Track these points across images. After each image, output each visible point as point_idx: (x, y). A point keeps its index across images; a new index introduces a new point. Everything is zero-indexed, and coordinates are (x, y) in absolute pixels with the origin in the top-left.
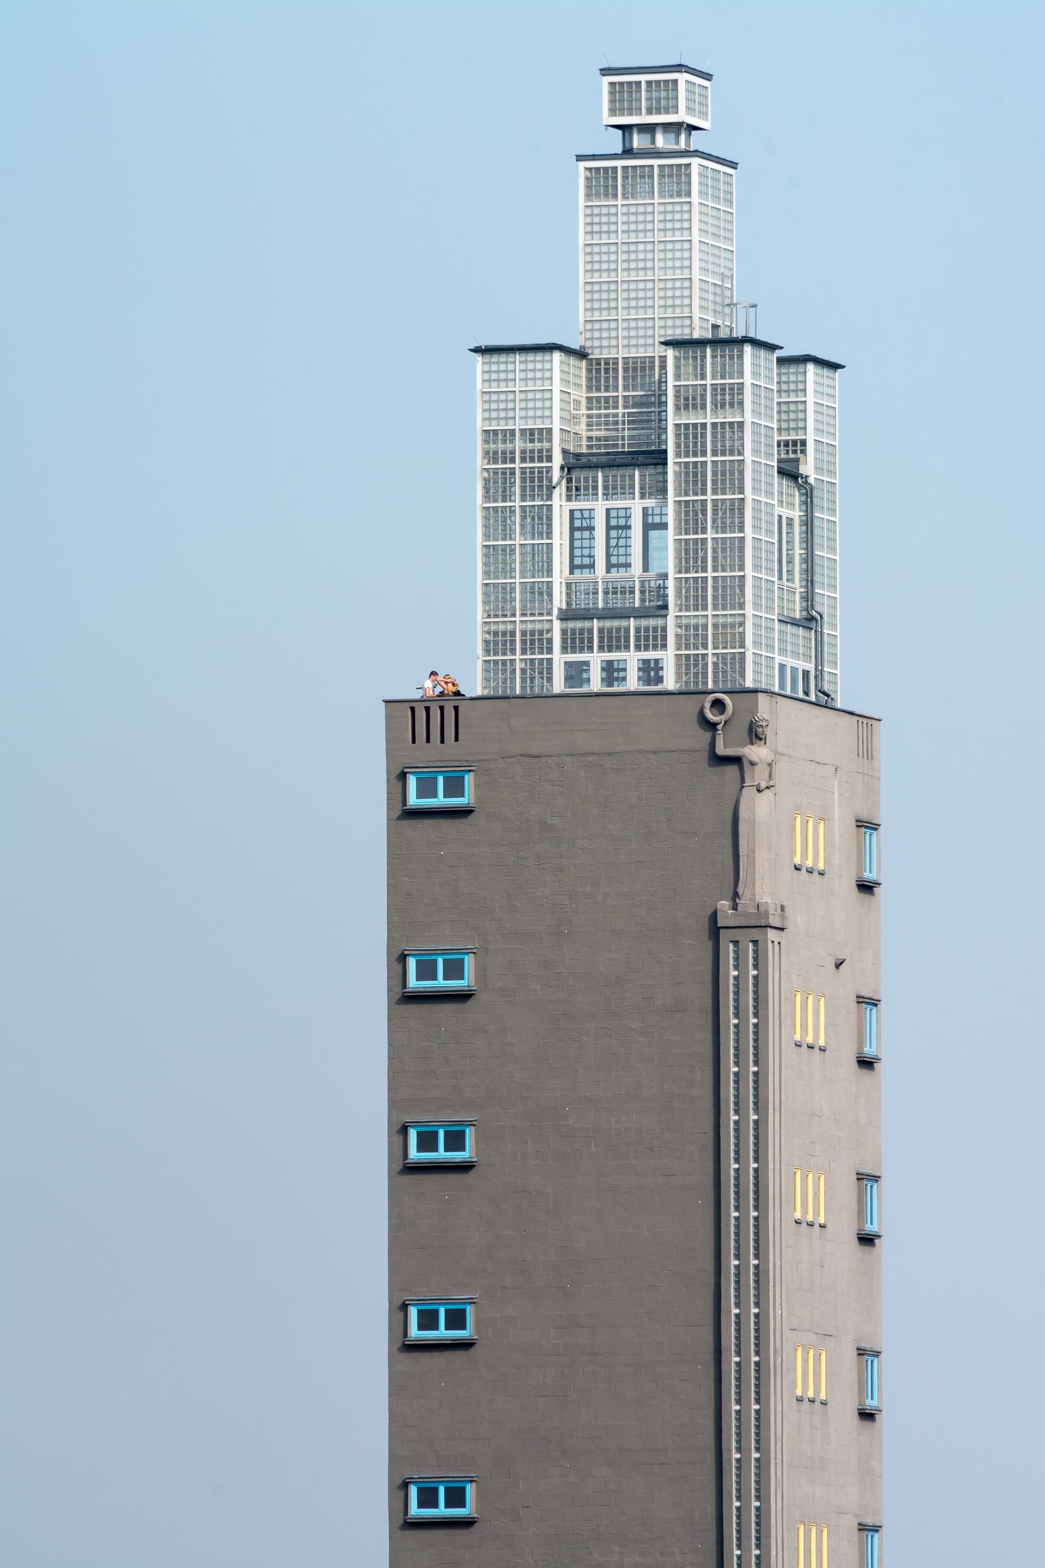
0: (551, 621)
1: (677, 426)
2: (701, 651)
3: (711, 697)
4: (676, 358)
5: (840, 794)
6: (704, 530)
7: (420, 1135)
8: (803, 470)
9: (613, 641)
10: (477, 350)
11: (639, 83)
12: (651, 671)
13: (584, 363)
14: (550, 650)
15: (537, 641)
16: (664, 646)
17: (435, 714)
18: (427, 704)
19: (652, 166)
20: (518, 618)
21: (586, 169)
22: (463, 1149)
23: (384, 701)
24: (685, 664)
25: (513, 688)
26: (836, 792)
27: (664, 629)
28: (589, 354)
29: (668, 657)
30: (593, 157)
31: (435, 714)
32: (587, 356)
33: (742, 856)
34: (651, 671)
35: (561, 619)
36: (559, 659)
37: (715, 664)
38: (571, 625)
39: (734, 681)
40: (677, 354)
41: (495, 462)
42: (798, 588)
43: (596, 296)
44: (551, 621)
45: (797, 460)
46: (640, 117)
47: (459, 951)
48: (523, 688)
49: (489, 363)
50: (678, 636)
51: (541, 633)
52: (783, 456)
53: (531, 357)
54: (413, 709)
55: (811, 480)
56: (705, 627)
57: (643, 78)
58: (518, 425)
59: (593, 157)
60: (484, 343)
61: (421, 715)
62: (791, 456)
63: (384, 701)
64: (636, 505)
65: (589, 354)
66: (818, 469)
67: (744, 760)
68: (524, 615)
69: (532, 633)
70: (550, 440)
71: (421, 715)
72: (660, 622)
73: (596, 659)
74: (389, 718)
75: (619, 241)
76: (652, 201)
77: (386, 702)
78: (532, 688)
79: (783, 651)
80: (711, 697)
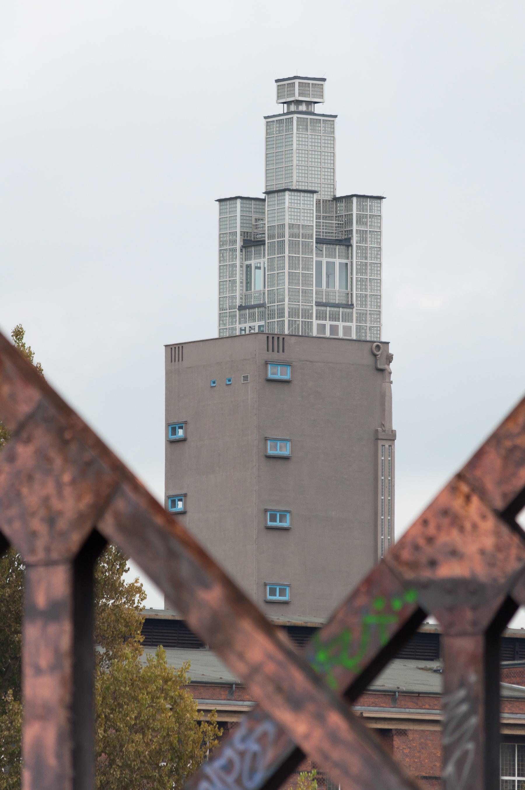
0: (312, 306)
3: (375, 344)
7: (271, 515)
9: (334, 317)
11: (309, 84)
12: (347, 330)
14: (312, 318)
15: (307, 314)
18: (273, 336)
19: (308, 118)
20: (301, 304)
22: (270, 521)
24: (359, 328)
25: (298, 332)
29: (353, 325)
34: (347, 330)
36: (315, 322)
38: (320, 308)
39: (308, 333)
43: (300, 171)
44: (312, 306)
48: (302, 333)
49: (291, 195)
51: (308, 310)
52: (246, 238)
53: (306, 194)
64: (337, 261)
73: (328, 323)
76: (307, 133)
78: (268, 330)
80: (375, 344)
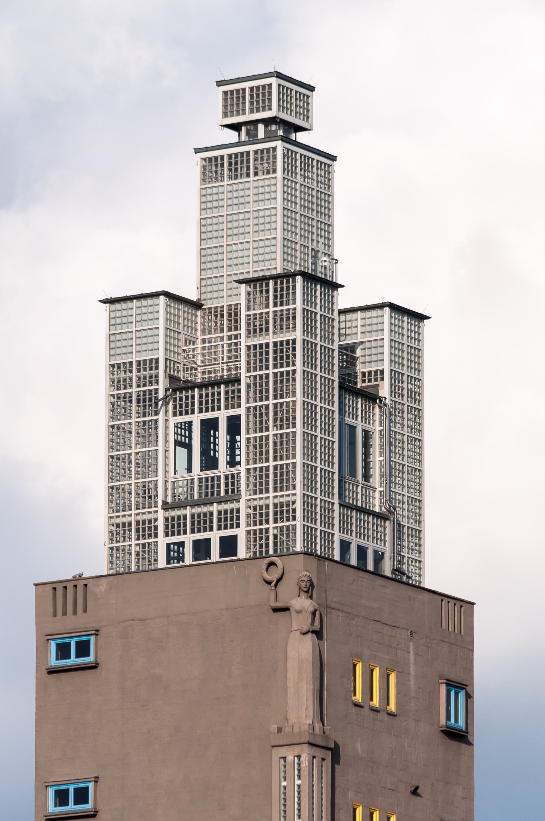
1: (249, 347)
2: (265, 526)
4: (249, 294)
5: (416, 654)
6: (267, 429)
8: (381, 393)
10: (105, 301)
13: (199, 313)
16: (238, 526)
17: (70, 591)
18: (64, 584)
21: (202, 159)
23: (35, 585)
26: (412, 652)
27: (238, 511)
28: (203, 305)
30: (207, 149)
31: (70, 591)
32: (202, 306)
33: (289, 688)
35: (164, 509)
36: (162, 541)
37: (275, 537)
40: (249, 289)
41: (118, 388)
42: (377, 488)
45: (378, 386)
46: (244, 116)
47: (85, 780)
50: (248, 516)
51: (150, 521)
54: (55, 589)
55: (388, 401)
56: (268, 506)
57: (247, 85)
58: (134, 358)
59: (207, 149)
60: (108, 296)
61: (60, 591)
62: (373, 383)
63: (35, 585)
65: (203, 305)
66: (393, 392)
67: (291, 609)
68: (137, 509)
69: (144, 522)
70: (157, 368)
71: (60, 591)
72: (233, 506)
74: (38, 598)
75: (225, 214)
77: (36, 585)
79: (359, 534)
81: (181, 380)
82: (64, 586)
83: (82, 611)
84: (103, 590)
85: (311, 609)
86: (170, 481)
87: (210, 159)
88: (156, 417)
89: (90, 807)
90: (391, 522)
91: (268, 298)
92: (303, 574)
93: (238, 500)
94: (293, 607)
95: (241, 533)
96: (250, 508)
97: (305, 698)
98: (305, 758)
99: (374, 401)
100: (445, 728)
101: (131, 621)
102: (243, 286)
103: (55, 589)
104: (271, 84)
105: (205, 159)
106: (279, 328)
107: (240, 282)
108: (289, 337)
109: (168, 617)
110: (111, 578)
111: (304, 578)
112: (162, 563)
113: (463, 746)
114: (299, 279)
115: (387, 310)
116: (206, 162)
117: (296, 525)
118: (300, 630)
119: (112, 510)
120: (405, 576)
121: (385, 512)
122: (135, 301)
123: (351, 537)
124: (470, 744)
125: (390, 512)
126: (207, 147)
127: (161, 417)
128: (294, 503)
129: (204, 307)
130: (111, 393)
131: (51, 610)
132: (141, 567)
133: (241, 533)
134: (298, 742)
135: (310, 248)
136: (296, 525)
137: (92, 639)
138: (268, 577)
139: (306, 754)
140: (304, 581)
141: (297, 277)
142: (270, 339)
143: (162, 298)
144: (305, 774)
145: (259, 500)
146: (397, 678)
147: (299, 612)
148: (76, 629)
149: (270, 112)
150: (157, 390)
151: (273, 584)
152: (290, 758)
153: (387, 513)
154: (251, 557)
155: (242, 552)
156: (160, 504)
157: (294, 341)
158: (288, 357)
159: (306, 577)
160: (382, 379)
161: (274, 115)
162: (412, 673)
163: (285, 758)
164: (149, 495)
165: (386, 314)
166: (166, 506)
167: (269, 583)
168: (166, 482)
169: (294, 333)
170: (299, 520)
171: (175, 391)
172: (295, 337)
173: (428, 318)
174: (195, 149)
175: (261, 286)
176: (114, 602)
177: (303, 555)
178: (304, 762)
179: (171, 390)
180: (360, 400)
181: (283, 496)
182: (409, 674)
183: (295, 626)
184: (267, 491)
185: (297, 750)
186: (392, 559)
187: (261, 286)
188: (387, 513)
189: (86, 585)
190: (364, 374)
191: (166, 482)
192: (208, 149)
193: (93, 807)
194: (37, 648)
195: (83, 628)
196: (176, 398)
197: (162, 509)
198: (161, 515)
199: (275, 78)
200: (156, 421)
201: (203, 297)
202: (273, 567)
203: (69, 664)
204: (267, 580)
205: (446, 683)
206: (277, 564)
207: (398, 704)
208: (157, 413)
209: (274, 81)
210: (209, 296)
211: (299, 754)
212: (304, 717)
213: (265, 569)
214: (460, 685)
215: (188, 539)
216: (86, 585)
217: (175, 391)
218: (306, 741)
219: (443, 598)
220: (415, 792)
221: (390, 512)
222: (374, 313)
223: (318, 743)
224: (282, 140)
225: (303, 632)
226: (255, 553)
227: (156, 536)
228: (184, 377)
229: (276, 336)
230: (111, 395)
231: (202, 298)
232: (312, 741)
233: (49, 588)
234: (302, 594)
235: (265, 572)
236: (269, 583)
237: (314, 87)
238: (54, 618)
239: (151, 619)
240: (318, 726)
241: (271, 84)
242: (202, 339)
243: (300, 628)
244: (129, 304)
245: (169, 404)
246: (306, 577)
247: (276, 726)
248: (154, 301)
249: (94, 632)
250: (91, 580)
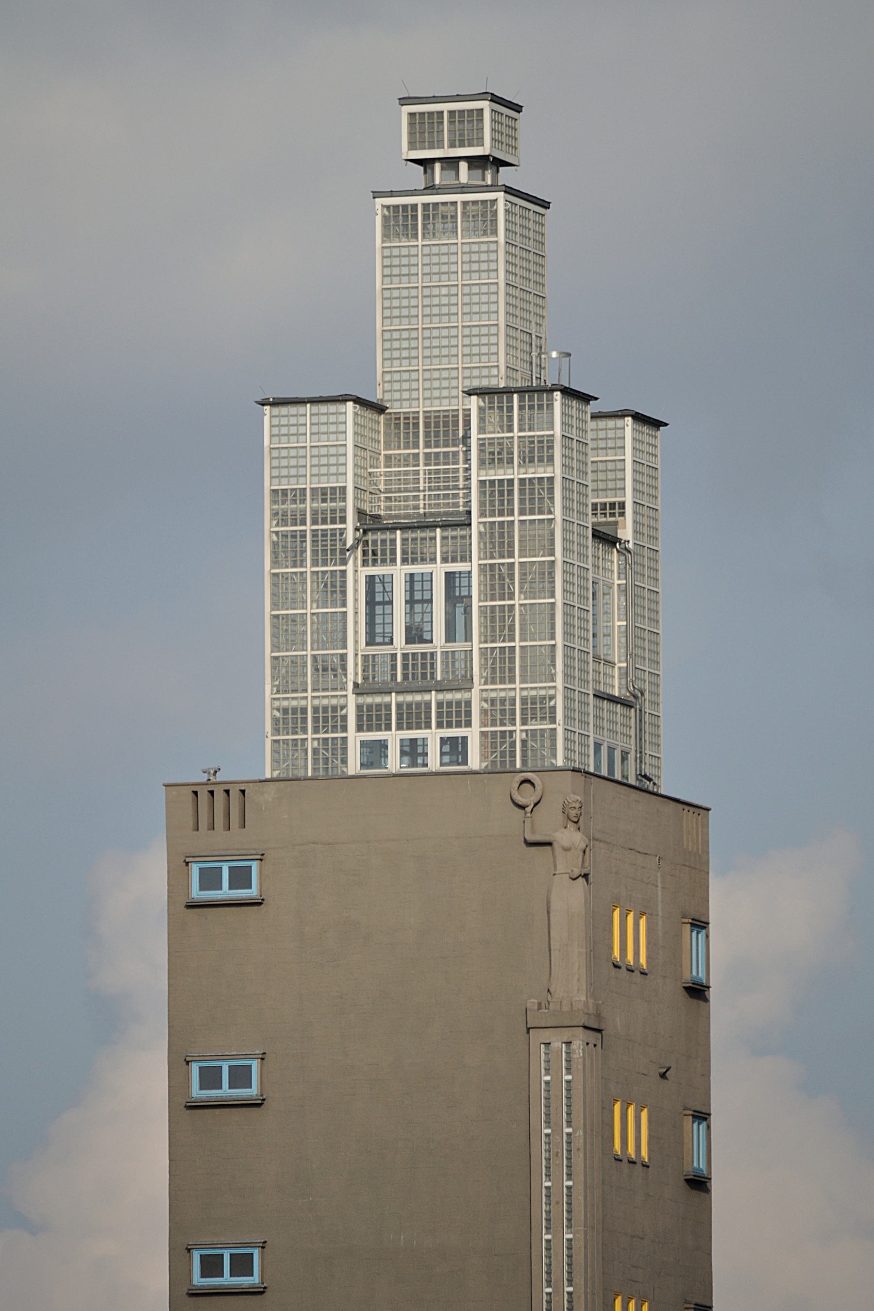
1: (482, 483)
16: (469, 724)
27: (468, 703)
30: (392, 194)
35: (356, 694)
36: (354, 738)
42: (616, 662)
50: (484, 712)
58: (308, 484)
61: (204, 797)
67: (555, 844)
69: (325, 709)
75: (420, 285)
81: (367, 515)
82: (210, 789)
83: (238, 826)
84: (270, 800)
85: (583, 846)
86: (360, 653)
87: (396, 207)
88: (343, 568)
89: (255, 1093)
90: (636, 711)
91: (510, 419)
92: (573, 799)
93: (470, 689)
94: (558, 843)
95: (473, 734)
96: (486, 701)
97: (577, 965)
98: (578, 1045)
99: (614, 544)
100: (691, 985)
101: (313, 845)
102: (474, 398)
103: (196, 793)
104: (482, 109)
105: (388, 207)
106: (528, 459)
107: (469, 393)
108: (542, 472)
109: (368, 842)
110: (282, 784)
111: (574, 805)
112: (353, 767)
113: (702, 1003)
114: (557, 395)
115: (629, 420)
116: (389, 212)
117: (555, 729)
118: (569, 873)
119: (275, 689)
120: (652, 783)
121: (628, 697)
122: (308, 405)
123: (602, 738)
124: (707, 1000)
125: (635, 697)
126: (391, 191)
127: (350, 567)
128: (552, 697)
129: (388, 411)
130: (272, 529)
131: (190, 823)
132: (330, 770)
133: (473, 734)
134: (569, 1025)
135: (534, 337)
136: (555, 729)
137: (255, 865)
138: (521, 800)
139: (580, 1040)
140: (575, 808)
141: (555, 393)
142: (515, 473)
143: (350, 404)
144: (579, 1067)
145: (499, 690)
146: (648, 922)
147: (567, 850)
148: (228, 850)
149: (481, 148)
150: (342, 532)
151: (529, 809)
152: (556, 1045)
153: (632, 699)
154: (489, 767)
155: (475, 761)
156: (350, 686)
157: (551, 480)
158: (541, 499)
159: (578, 803)
160: (622, 514)
161: (487, 154)
162: (660, 914)
163: (548, 1044)
164: (511, 740)
165: (627, 425)
166: (358, 690)
167: (522, 807)
168: (356, 655)
169: (550, 469)
170: (561, 723)
171: (365, 532)
172: (552, 475)
173: (666, 425)
174: (373, 192)
175: (500, 401)
176: (286, 816)
177: (570, 772)
178: (577, 1052)
179: (361, 530)
180: (601, 545)
181: (537, 688)
182: (657, 915)
183: (561, 868)
184: (512, 680)
185: (566, 1034)
186: (638, 761)
187: (500, 401)
188: (632, 699)
189: (243, 792)
190: (595, 506)
191: (356, 655)
192: (389, 194)
193: (259, 1094)
194: (168, 872)
195: (239, 849)
196: (367, 541)
197: (353, 693)
198: (352, 701)
199: (488, 103)
200: (344, 572)
201: (387, 396)
202: (527, 786)
203: (219, 897)
204: (520, 803)
205: (690, 923)
206: (535, 783)
207: (649, 958)
208: (344, 562)
209: (485, 105)
210: (397, 396)
211: (569, 1041)
212: (576, 991)
213: (516, 789)
214: (698, 923)
215: (394, 738)
216: (243, 792)
217: (365, 532)
218: (581, 1024)
219: (684, 806)
220: (663, 1076)
221: (635, 697)
222: (611, 423)
223: (592, 1026)
224: (505, 192)
225: (574, 877)
226: (493, 762)
227: (344, 729)
228: (371, 511)
229: (523, 470)
230: (273, 532)
231: (386, 398)
232: (587, 1025)
233: (188, 791)
234: (570, 825)
235: (517, 793)
236: (522, 807)
237: (522, 107)
238: (195, 832)
239: (343, 844)
240: (591, 1001)
241: (482, 109)
242: (385, 455)
243: (570, 871)
244: (301, 409)
245: (357, 548)
246: (578, 803)
247: (536, 1001)
248: (341, 407)
249: (259, 857)
250: (251, 784)
